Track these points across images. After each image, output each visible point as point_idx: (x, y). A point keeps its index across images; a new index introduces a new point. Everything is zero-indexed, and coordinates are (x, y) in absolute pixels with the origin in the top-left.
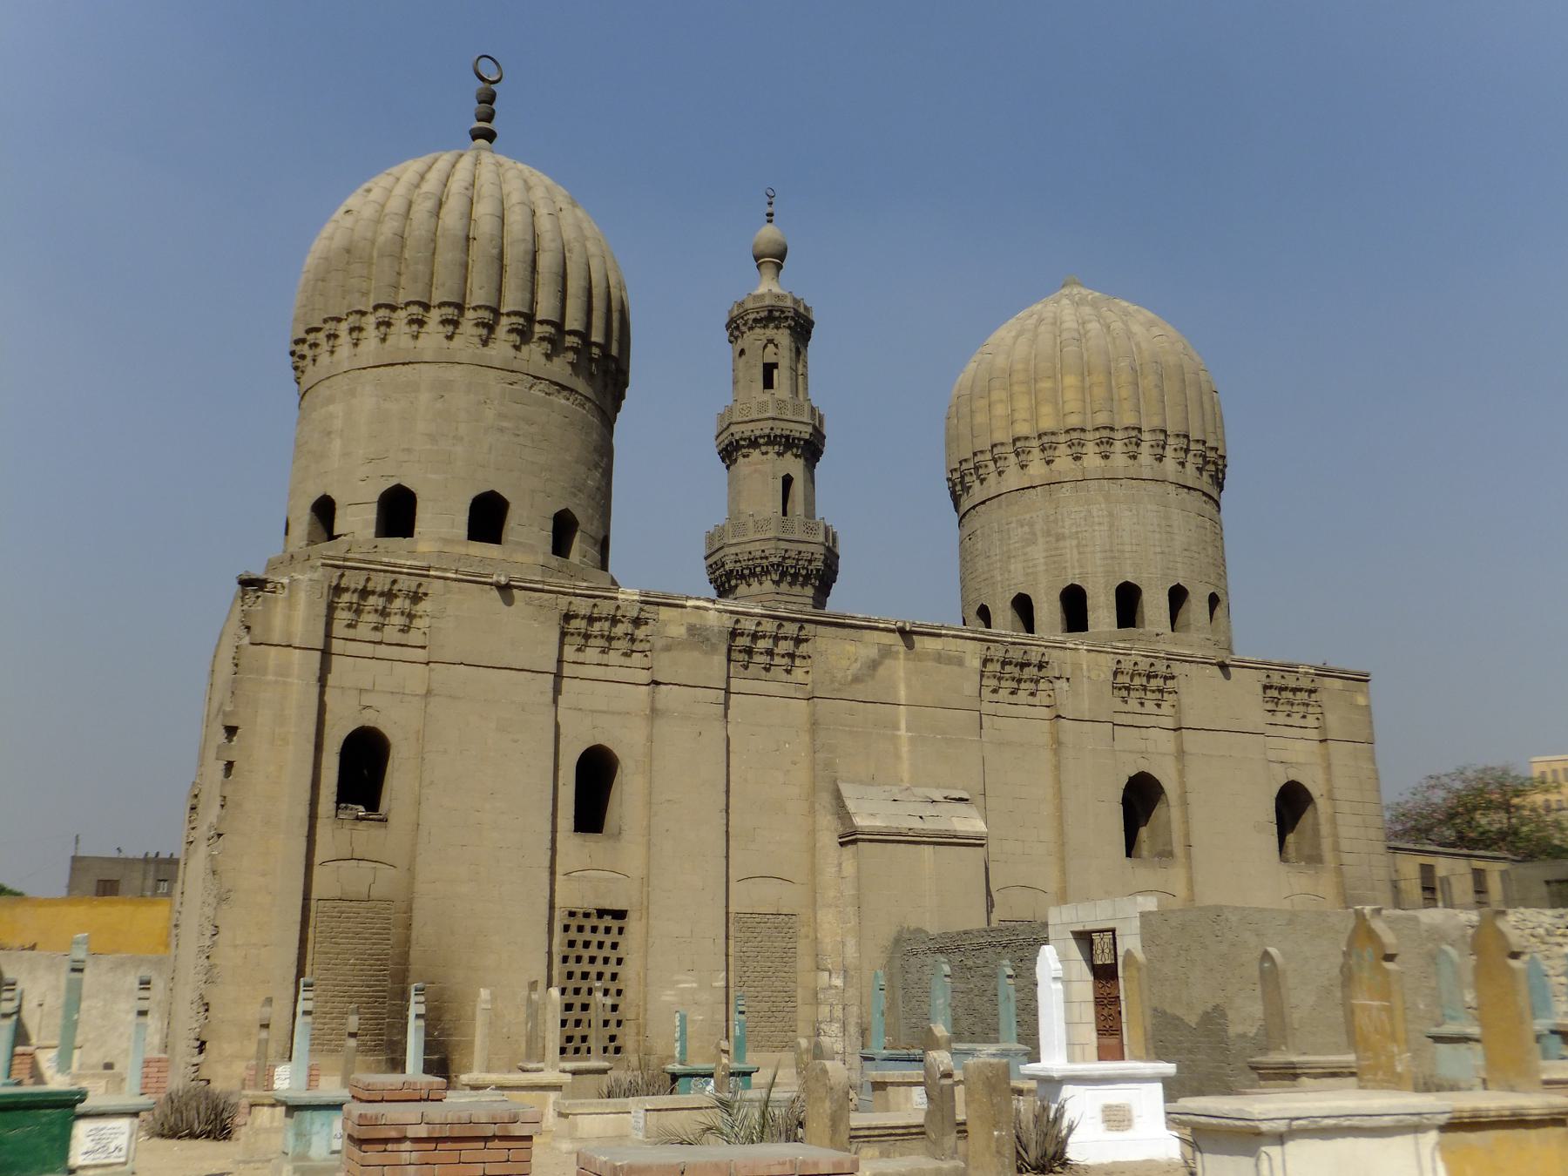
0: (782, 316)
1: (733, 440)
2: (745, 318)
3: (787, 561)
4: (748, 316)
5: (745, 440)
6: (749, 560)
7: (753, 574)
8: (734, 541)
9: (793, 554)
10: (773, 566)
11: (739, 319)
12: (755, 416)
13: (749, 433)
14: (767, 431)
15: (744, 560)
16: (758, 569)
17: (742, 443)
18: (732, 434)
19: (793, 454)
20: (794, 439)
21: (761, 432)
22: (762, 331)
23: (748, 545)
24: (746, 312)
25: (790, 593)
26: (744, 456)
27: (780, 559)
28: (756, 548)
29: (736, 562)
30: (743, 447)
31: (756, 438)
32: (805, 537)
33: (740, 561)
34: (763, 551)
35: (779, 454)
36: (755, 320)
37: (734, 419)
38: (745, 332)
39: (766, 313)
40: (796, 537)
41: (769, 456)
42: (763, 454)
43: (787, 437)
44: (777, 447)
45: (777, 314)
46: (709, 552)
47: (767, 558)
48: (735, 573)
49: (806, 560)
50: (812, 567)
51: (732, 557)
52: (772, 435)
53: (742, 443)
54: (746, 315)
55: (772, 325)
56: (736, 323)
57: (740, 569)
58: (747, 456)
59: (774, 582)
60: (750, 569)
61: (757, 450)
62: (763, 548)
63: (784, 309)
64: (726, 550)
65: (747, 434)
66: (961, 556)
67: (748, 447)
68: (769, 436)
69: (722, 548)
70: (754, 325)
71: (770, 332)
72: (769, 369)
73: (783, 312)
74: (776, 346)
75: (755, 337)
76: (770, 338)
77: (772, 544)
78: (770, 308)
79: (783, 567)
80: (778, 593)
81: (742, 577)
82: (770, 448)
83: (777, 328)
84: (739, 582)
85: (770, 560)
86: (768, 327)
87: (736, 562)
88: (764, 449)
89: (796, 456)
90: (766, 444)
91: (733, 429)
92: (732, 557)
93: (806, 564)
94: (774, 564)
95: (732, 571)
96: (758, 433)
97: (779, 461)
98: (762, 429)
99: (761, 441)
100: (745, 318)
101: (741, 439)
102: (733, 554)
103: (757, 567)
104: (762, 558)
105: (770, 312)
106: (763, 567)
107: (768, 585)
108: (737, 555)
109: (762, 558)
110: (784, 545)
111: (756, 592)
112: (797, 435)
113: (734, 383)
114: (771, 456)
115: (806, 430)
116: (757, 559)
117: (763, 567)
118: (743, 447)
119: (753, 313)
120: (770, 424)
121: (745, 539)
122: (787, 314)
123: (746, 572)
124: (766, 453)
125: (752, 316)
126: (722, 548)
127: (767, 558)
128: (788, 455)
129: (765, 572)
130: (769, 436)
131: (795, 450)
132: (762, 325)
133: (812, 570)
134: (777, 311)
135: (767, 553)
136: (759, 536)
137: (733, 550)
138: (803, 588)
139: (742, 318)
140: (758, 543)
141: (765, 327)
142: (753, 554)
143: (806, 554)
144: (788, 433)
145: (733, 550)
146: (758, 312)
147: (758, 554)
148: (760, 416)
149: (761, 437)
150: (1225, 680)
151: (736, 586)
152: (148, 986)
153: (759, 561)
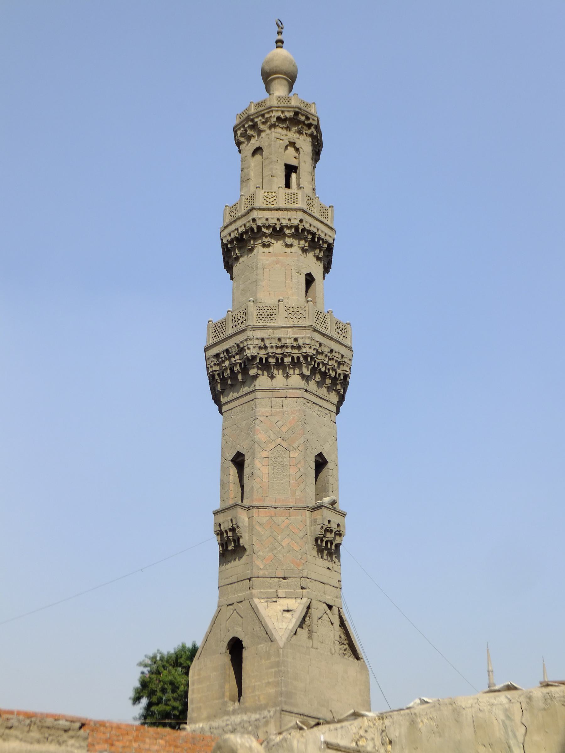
0: (306, 122)
1: (255, 227)
2: (267, 116)
3: (319, 357)
4: (271, 114)
5: (268, 227)
6: (277, 347)
7: (280, 365)
8: (260, 324)
9: (326, 350)
10: (305, 358)
11: (257, 117)
12: (282, 205)
13: (275, 221)
14: (296, 222)
15: (272, 347)
16: (287, 360)
17: (264, 230)
18: (254, 220)
19: (314, 256)
20: (319, 239)
21: (289, 223)
22: (284, 132)
23: (276, 331)
24: (270, 109)
25: (317, 394)
26: (264, 246)
27: (314, 352)
28: (288, 336)
29: (260, 348)
30: (265, 235)
31: (282, 228)
32: (335, 335)
33: (265, 348)
34: (296, 340)
35: (304, 250)
36: (279, 119)
37: (257, 204)
38: (264, 131)
39: (292, 114)
40: (328, 332)
41: (294, 249)
42: (287, 246)
43: (314, 234)
44: (302, 243)
45: (303, 118)
46: (211, 342)
47: (299, 348)
48: (258, 360)
49: (336, 361)
50: (341, 372)
51: (256, 342)
52: (301, 227)
53: (264, 230)
54: (268, 113)
55: (294, 129)
56: (252, 120)
57: (264, 357)
58: (269, 246)
59: (303, 376)
60: (277, 359)
61: (280, 243)
62: (296, 336)
63: (309, 116)
64: (250, 334)
65: (272, 222)
66: (221, 497)
67: (271, 236)
68: (297, 228)
69: (243, 331)
70: (277, 124)
71: (292, 135)
72: (290, 169)
73: (308, 118)
74: (297, 150)
75: (278, 135)
76: (292, 140)
77: (309, 333)
78: (297, 110)
79: (315, 362)
80: (306, 391)
81: (265, 366)
82: (295, 242)
83: (300, 132)
84: (260, 372)
85: (304, 350)
86: (290, 130)
87: (260, 348)
88: (289, 241)
89: (318, 258)
90: (292, 236)
91: (255, 214)
92: (256, 342)
93: (336, 365)
94: (308, 356)
95: (254, 358)
96: (284, 222)
97: (302, 257)
98: (290, 220)
99: (287, 232)
100: (267, 116)
101: (264, 226)
102: (257, 339)
103: (286, 356)
104: (293, 347)
105: (296, 113)
106: (293, 358)
107: (295, 379)
108: (263, 340)
109: (293, 347)
110: (318, 337)
111: (280, 386)
112: (322, 236)
113: (242, 182)
114: (296, 249)
115: (330, 235)
116: (287, 347)
117: (293, 358)
118: (265, 235)
119: (277, 111)
120: (300, 215)
121: (273, 324)
122: (311, 121)
123: (272, 361)
124: (291, 245)
125: (276, 114)
126: (243, 331)
127: (299, 348)
128: (311, 255)
129: (296, 364)
130: (297, 228)
131: (317, 251)
132: (284, 126)
133: (340, 374)
134: (303, 115)
135: (300, 342)
136: (290, 323)
137: (259, 334)
138: (328, 392)
139: (263, 116)
140: (290, 330)
141: (287, 128)
142: (283, 341)
143: (336, 355)
144: (315, 230)
145: (259, 334)
146: (283, 112)
147: (290, 342)
148: (288, 206)
149: (290, 228)
150: (243, 641)
151: (256, 377)
152: (344, 516)
153: (289, 350)
